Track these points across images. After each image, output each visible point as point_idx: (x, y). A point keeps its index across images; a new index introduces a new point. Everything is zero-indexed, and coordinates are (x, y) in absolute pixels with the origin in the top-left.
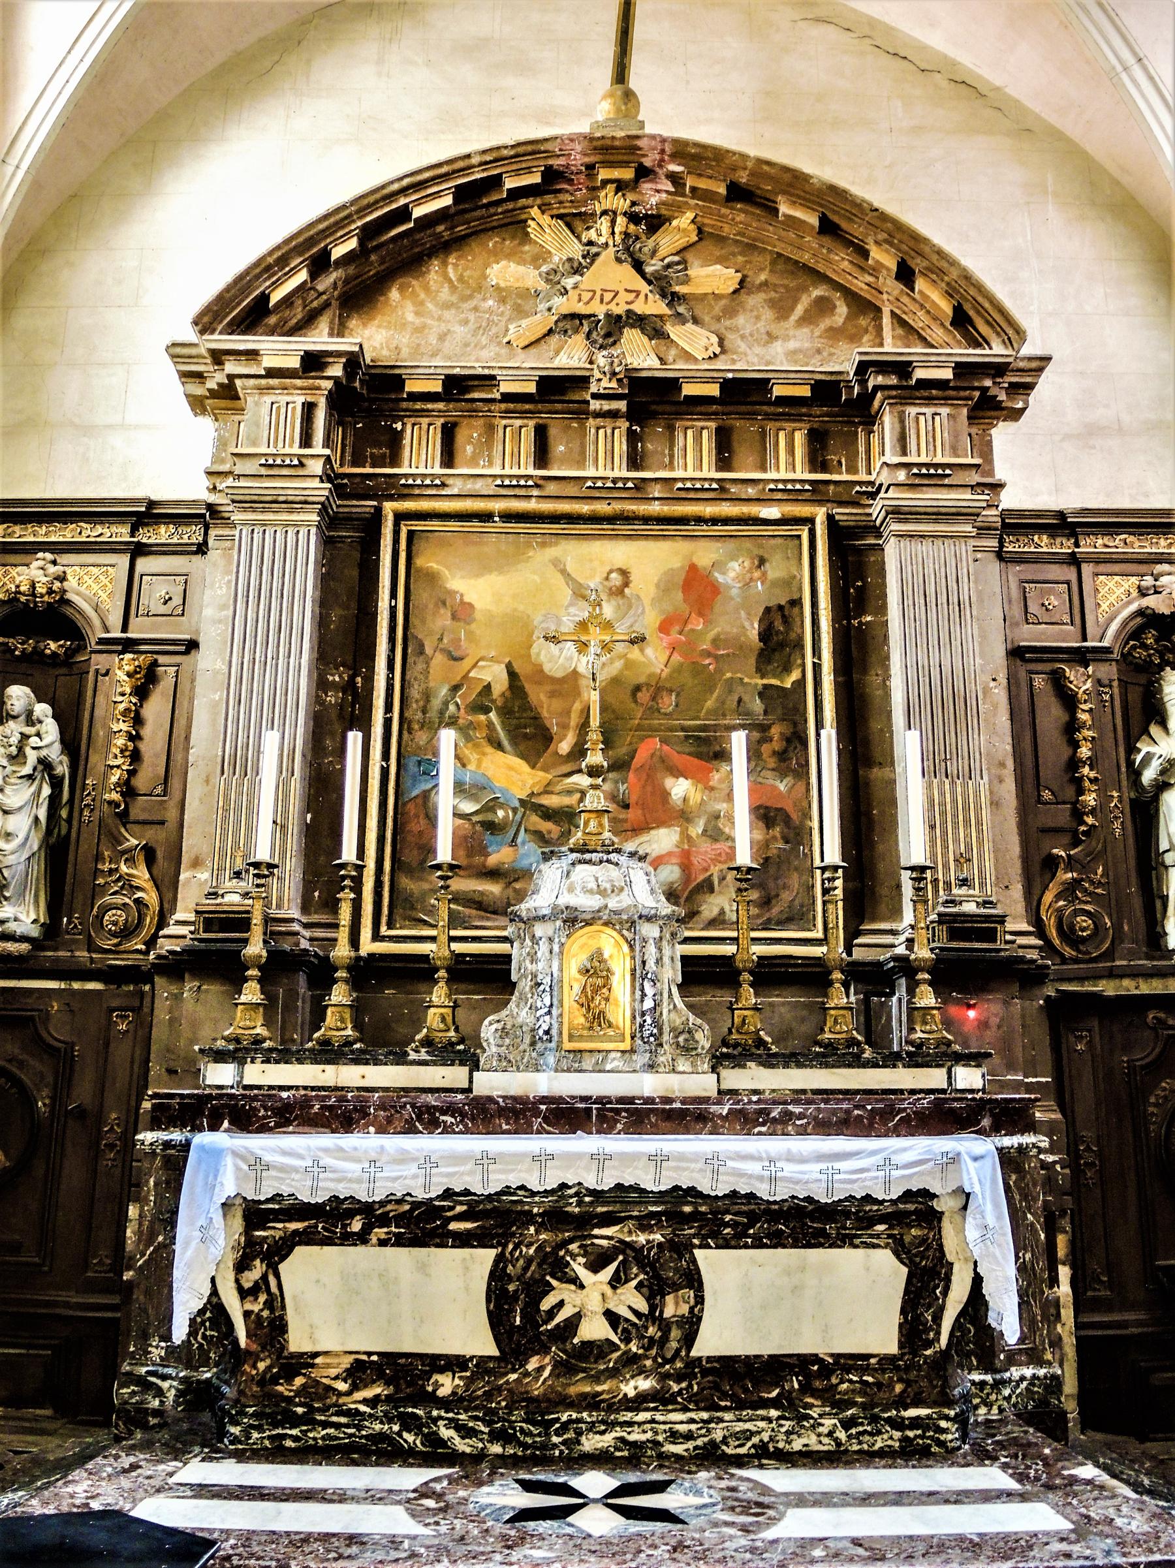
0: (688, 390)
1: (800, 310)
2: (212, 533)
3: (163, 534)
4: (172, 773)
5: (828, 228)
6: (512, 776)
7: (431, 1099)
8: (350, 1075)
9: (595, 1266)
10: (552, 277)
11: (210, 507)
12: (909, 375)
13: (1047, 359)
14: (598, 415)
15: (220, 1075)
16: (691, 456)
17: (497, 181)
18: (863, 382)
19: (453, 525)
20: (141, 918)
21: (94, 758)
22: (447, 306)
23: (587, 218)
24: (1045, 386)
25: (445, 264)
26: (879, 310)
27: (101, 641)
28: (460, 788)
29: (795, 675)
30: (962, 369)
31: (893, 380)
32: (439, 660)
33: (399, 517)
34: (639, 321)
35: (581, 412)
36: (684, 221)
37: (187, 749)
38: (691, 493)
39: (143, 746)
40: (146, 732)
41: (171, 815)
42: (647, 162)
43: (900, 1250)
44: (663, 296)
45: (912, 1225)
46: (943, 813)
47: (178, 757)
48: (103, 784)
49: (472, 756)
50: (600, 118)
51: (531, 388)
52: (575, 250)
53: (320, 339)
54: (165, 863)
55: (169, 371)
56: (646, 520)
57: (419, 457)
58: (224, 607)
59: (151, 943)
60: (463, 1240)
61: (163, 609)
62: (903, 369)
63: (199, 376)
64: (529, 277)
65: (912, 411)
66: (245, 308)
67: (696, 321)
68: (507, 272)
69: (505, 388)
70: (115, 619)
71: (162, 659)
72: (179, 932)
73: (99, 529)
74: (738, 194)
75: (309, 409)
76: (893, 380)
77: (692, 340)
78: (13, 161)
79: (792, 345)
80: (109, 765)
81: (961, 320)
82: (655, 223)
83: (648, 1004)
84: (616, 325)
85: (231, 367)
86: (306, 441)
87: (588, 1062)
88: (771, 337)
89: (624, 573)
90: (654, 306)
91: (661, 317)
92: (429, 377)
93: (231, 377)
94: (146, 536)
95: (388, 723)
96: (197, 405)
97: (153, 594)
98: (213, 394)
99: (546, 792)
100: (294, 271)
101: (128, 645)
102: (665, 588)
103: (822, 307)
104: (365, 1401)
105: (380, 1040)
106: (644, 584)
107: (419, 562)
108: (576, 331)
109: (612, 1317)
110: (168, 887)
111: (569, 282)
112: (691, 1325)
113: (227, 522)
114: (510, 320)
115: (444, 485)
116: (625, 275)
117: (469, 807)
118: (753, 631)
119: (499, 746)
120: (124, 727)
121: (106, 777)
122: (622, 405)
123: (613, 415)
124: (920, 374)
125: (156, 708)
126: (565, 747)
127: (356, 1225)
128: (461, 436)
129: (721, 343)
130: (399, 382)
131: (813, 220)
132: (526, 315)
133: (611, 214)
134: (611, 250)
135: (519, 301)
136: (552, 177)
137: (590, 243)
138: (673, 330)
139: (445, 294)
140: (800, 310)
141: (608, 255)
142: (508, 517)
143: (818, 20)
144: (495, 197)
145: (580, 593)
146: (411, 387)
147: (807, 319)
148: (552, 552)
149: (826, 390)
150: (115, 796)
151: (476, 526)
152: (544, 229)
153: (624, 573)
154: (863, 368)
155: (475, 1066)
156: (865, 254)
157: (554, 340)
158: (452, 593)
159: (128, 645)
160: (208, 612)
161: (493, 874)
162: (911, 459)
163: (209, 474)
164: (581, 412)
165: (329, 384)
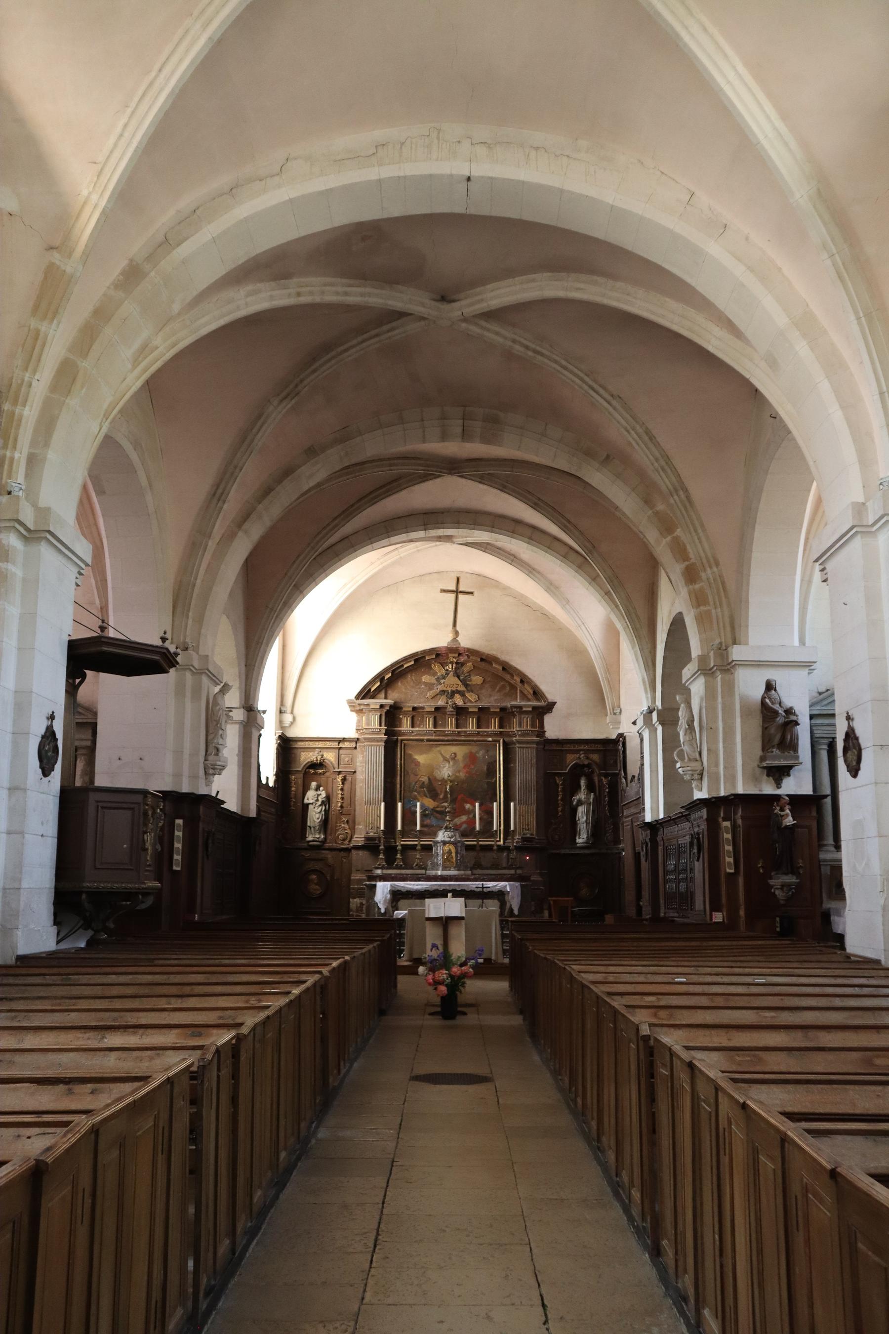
0: (470, 710)
3: (346, 745)
4: (352, 802)
5: (504, 669)
6: (430, 803)
8: (403, 871)
10: (438, 680)
15: (379, 872)
16: (471, 726)
17: (425, 657)
22: (413, 687)
32: (412, 776)
33: (402, 740)
34: (459, 692)
35: (445, 713)
38: (472, 734)
39: (345, 796)
41: (352, 812)
43: (499, 900)
45: (500, 895)
48: (336, 806)
54: (352, 824)
57: (405, 725)
59: (350, 841)
64: (433, 680)
66: (366, 693)
67: (472, 691)
68: (426, 678)
70: (336, 766)
72: (359, 838)
74: (482, 660)
75: (381, 716)
80: (337, 803)
82: (463, 664)
84: (453, 694)
86: (380, 725)
88: (491, 696)
90: (462, 688)
94: (341, 745)
97: (345, 759)
101: (339, 773)
102: (464, 757)
103: (503, 687)
105: (408, 866)
106: (460, 757)
110: (353, 830)
111: (442, 681)
118: (485, 768)
125: (347, 787)
126: (441, 797)
128: (416, 719)
130: (401, 708)
131: (500, 668)
133: (452, 663)
135: (430, 686)
136: (438, 655)
138: (467, 695)
139: (412, 683)
140: (498, 688)
141: (452, 673)
142: (428, 740)
146: (404, 709)
147: (499, 691)
148: (438, 749)
149: (503, 709)
152: (436, 667)
153: (455, 754)
155: (426, 869)
159: (339, 773)
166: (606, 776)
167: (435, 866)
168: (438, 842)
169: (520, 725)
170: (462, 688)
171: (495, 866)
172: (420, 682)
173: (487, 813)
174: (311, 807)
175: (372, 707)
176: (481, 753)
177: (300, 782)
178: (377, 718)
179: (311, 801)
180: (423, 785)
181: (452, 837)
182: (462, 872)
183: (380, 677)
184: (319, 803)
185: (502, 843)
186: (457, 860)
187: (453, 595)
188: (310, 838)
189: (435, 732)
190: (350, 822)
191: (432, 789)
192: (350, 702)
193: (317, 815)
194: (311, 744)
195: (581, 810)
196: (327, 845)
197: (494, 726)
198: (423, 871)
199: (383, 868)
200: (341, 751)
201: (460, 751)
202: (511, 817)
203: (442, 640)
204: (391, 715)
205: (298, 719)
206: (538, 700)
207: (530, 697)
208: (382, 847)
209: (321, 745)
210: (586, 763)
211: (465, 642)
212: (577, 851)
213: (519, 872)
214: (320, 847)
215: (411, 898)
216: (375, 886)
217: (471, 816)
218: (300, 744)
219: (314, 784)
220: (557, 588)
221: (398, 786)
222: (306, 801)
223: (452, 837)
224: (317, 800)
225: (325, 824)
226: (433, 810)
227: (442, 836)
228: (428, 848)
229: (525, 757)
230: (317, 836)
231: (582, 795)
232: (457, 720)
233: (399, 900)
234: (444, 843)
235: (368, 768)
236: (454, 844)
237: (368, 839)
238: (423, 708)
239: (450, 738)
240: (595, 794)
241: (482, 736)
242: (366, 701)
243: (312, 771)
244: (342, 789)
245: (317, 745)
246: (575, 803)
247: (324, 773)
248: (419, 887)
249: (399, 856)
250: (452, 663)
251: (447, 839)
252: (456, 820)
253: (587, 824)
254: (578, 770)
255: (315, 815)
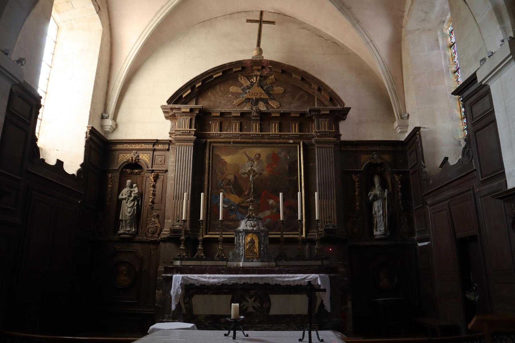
0: (273, 115)
1: (297, 96)
2: (170, 146)
3: (160, 147)
5: (303, 79)
6: (235, 199)
7: (220, 268)
8: (203, 263)
9: (251, 298)
10: (244, 90)
11: (170, 141)
12: (320, 112)
13: (350, 108)
14: (253, 120)
15: (178, 263)
16: (274, 130)
17: (232, 69)
18: (310, 114)
19: (222, 145)
20: (157, 230)
21: (146, 196)
23: (251, 77)
24: (350, 113)
25: (220, 87)
26: (314, 97)
27: (147, 170)
28: (224, 202)
29: (296, 177)
30: (331, 111)
31: (317, 113)
33: (210, 143)
34: (262, 100)
35: (250, 119)
36: (272, 77)
37: (166, 193)
38: (274, 137)
39: (156, 193)
40: (157, 189)
42: (264, 65)
44: (267, 94)
45: (310, 289)
46: (326, 207)
47: (164, 195)
49: (227, 195)
50: (254, 55)
51: (239, 115)
52: (249, 83)
53: (193, 105)
54: (161, 218)
55: (161, 111)
56: (264, 143)
57: (214, 130)
58: (173, 163)
59: (159, 235)
60: (226, 293)
61: (160, 163)
62: (319, 111)
63: (167, 112)
65: (321, 120)
66: (177, 98)
67: (274, 100)
68: (233, 89)
69: (233, 115)
71: (160, 174)
72: (166, 232)
73: (146, 146)
74: (283, 72)
75: (191, 119)
76: (317, 113)
77: (274, 104)
78: (126, 64)
79: (295, 105)
80: (148, 198)
81: (331, 99)
82: (266, 77)
83: (262, 249)
84: (257, 101)
85: (174, 111)
86: (190, 128)
87: (250, 260)
88: (291, 103)
89: (259, 155)
90: (265, 96)
91: (267, 99)
92: (217, 112)
93: (175, 113)
94: (156, 147)
95: (208, 188)
96: (167, 118)
97: (158, 159)
98: (170, 116)
99: (243, 203)
100: (188, 90)
104: (208, 323)
105: (209, 256)
106: (263, 157)
107: (215, 152)
108: (249, 102)
109: (253, 307)
110: (162, 223)
111: (247, 91)
112: (269, 309)
113: (174, 144)
114: (234, 100)
115: (220, 136)
116: (260, 90)
117: (226, 206)
119: (232, 193)
120: (152, 189)
121: (149, 200)
122: (259, 118)
123: (257, 120)
124: (322, 112)
125: (159, 184)
126: (246, 193)
127: (206, 291)
129: (280, 104)
130: (211, 113)
131: (300, 78)
132: (238, 98)
133: (256, 76)
134: (256, 84)
135: (236, 95)
136: (243, 68)
137: (252, 82)
138: (270, 103)
140: (297, 96)
142: (234, 142)
143: (303, 28)
144: (231, 73)
145: (250, 159)
148: (244, 150)
149: (303, 115)
150: (151, 204)
151: (227, 145)
153: (259, 155)
154: (310, 111)
155: (228, 261)
156: (311, 85)
157: (244, 104)
158: (222, 159)
159: (153, 171)
160: (170, 164)
161: (232, 220)
162: (321, 130)
163: (170, 133)
164: (250, 119)
165: (195, 115)
166: (398, 173)
167: (237, 257)
168: (240, 232)
169: (318, 128)
170: (265, 96)
171: (300, 257)
172: (228, 92)
173: (291, 208)
174: (124, 202)
175: (183, 110)
176: (283, 153)
177: (117, 180)
178: (188, 122)
179: (124, 197)
180: (229, 182)
181: (255, 226)
182: (266, 263)
183: (191, 85)
184: (132, 198)
185: (304, 235)
186: (260, 250)
187: (257, 25)
188: (121, 231)
189: (241, 135)
190: (160, 216)
191: (236, 186)
192: (163, 107)
193: (129, 210)
194: (129, 146)
195: (377, 206)
196: (138, 238)
197: (294, 130)
198: (224, 263)
199: (181, 259)
200: (155, 153)
201: (264, 152)
202: (313, 205)
203: (247, 54)
204: (201, 119)
205: (120, 127)
206: (334, 105)
207: (326, 103)
208: (183, 238)
209: (138, 147)
210: (379, 162)
211: (267, 56)
212: (376, 243)
213: (326, 262)
214: (130, 239)
215: (207, 293)
216: (171, 278)
217: (274, 211)
218: (119, 147)
219: (129, 181)
220: (348, 8)
221: (206, 183)
222: (120, 197)
223: (255, 226)
224: (130, 196)
225: (137, 217)
226: (239, 205)
227: (243, 225)
228: (230, 241)
229: (323, 156)
230: (128, 229)
231: (377, 191)
232: (261, 125)
233: (192, 296)
234: (247, 232)
235: (177, 167)
236: (257, 233)
237: (173, 231)
238: (230, 113)
239: (254, 140)
240: (388, 190)
241: (283, 139)
242: (177, 106)
243: (129, 171)
244: (154, 186)
245: (133, 146)
246: (371, 198)
247: (139, 173)
248: (216, 280)
249: (200, 247)
250: (256, 76)
251: (249, 228)
252: (260, 214)
253: (384, 217)
254: (373, 169)
255: (127, 209)
